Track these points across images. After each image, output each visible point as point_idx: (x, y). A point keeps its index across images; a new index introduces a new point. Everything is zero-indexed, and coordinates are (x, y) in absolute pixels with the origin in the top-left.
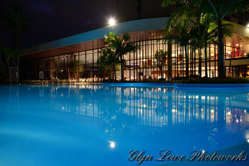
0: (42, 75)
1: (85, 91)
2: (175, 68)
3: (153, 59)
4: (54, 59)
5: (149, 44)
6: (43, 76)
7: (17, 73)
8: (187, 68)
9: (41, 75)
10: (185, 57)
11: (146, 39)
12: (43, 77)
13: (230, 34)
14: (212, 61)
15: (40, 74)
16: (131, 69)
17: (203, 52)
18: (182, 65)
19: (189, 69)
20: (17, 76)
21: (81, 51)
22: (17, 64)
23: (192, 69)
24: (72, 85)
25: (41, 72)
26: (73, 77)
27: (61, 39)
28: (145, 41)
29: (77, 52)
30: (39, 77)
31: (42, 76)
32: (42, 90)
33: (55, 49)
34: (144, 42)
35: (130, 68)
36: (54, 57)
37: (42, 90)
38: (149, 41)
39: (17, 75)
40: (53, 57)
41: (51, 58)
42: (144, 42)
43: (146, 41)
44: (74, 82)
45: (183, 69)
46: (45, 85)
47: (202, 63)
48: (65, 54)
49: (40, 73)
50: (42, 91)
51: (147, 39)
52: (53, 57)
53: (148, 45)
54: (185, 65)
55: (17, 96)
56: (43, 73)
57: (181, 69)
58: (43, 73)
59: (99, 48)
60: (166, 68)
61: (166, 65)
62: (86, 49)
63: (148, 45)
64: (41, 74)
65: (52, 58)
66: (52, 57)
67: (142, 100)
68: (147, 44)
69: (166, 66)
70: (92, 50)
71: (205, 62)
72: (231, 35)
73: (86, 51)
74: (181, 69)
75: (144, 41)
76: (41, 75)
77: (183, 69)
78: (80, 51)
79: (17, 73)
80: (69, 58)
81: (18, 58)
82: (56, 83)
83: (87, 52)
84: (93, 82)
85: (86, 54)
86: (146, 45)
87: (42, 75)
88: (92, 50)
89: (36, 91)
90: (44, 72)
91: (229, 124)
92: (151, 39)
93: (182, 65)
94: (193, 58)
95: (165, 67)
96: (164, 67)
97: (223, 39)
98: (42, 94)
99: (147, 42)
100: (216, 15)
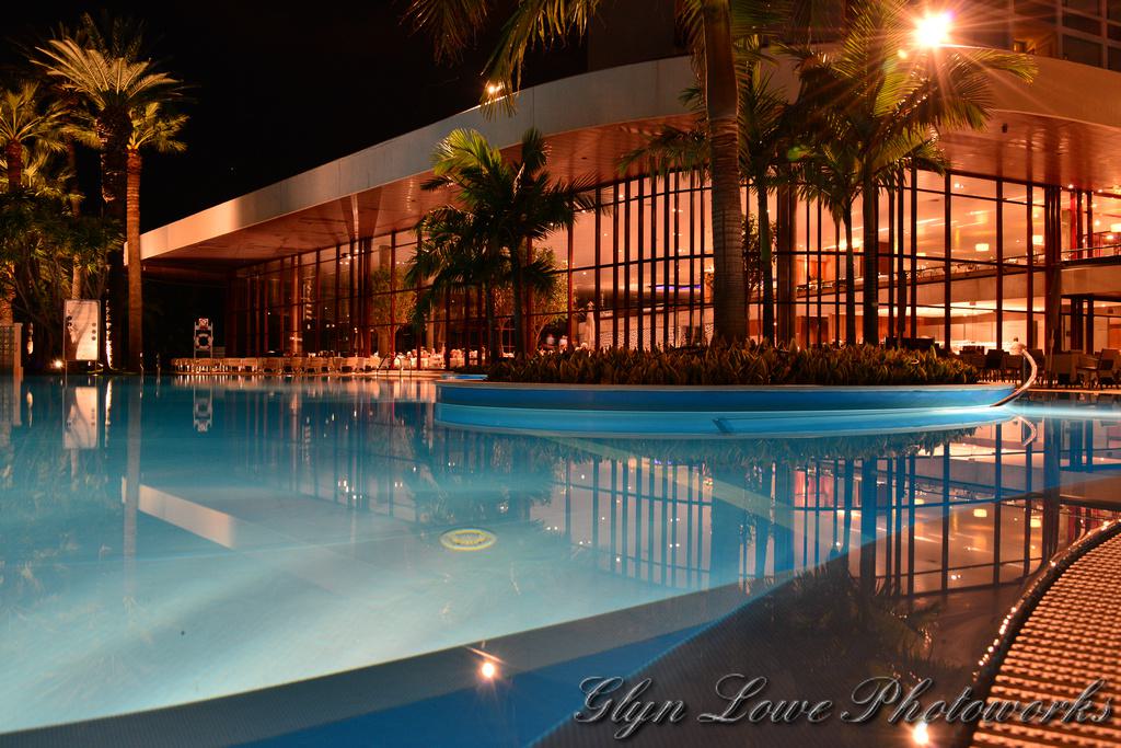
0: (206, 335)
2: (837, 303)
3: (699, 259)
4: (300, 266)
5: (680, 189)
6: (211, 340)
10: (712, 252)
13: (977, 112)
14: (1020, 269)
17: (1038, 219)
19: (1043, 309)
23: (896, 310)
24: (361, 379)
25: (204, 322)
26: (372, 347)
27: (294, 178)
30: (193, 342)
31: (204, 341)
32: (205, 400)
34: (634, 185)
35: (653, 309)
37: (204, 401)
40: (622, 186)
42: (634, 185)
44: (369, 369)
45: (913, 311)
47: (880, 291)
49: (197, 328)
50: (203, 408)
52: (622, 186)
53: (677, 192)
54: (862, 293)
56: (210, 328)
57: (891, 312)
58: (210, 328)
60: (808, 303)
61: (810, 293)
63: (677, 192)
64: (203, 332)
68: (672, 189)
69: (808, 296)
71: (994, 276)
72: (982, 117)
74: (891, 312)
77: (913, 311)
83: (398, 235)
86: (667, 193)
87: (206, 335)
96: (811, 299)
98: (203, 419)
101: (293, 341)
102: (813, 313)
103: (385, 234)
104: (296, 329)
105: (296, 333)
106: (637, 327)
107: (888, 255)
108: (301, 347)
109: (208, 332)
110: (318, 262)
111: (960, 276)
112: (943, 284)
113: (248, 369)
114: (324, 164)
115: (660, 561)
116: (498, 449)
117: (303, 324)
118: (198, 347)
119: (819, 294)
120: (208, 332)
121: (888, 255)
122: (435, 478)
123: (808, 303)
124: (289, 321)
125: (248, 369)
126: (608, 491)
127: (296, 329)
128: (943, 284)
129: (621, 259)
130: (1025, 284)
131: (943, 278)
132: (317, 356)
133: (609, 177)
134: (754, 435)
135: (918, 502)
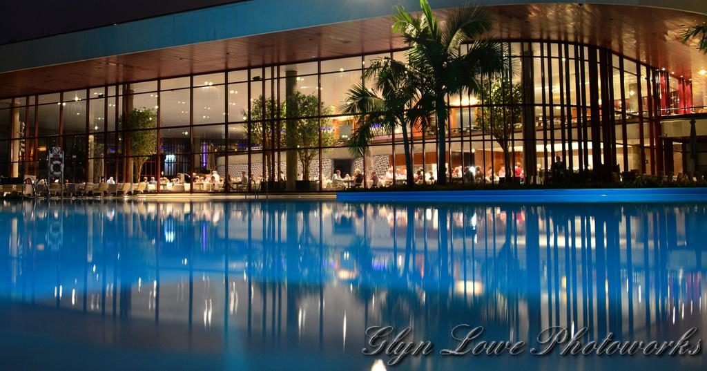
0: (58, 162)
1: (189, 229)
8: (530, 143)
9: (55, 162)
11: (273, 59)
15: (53, 159)
16: (645, 124)
18: (548, 133)
21: (169, 75)
28: (270, 68)
29: (102, 86)
33: (65, 65)
34: (268, 70)
38: (109, 88)
43: (272, 65)
51: (275, 61)
56: (61, 156)
58: (61, 156)
59: (253, 64)
60: (462, 141)
62: (192, 70)
67: (641, 246)
69: (462, 137)
70: (224, 73)
73: (192, 75)
75: (268, 66)
76: (55, 162)
78: (163, 75)
80: (112, 105)
84: (227, 189)
85: (192, 88)
86: (273, 79)
88: (224, 73)
90: (64, 149)
91: (308, 295)
92: (391, 47)
93: (548, 133)
94: (584, 107)
95: (468, 138)
96: (465, 139)
99: (276, 68)
102: (466, 150)
107: (530, 105)
109: (60, 160)
111: (87, 304)
112: (542, 132)
115: (575, 104)
119: (449, 138)
120: (60, 160)
121: (530, 105)
123: (462, 141)
126: (516, 140)
128: (542, 132)
129: (276, 81)
130: (638, 130)
131: (537, 142)
134: (437, 192)
135: (559, 108)
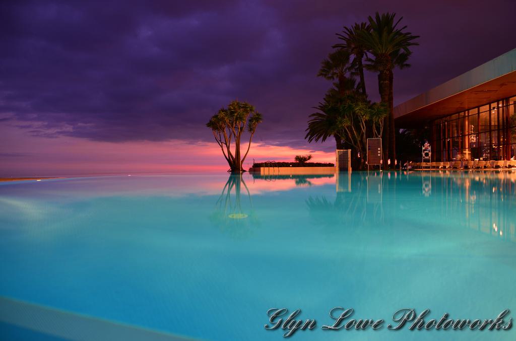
0: (428, 152)
4: (468, 116)
6: (430, 154)
7: (379, 149)
9: (425, 152)
12: (430, 155)
15: (424, 150)
20: (379, 155)
22: (379, 134)
30: (422, 155)
31: (427, 155)
36: (468, 110)
37: (427, 183)
39: (380, 153)
40: (467, 112)
41: (462, 114)
46: (445, 172)
48: (481, 106)
49: (423, 148)
52: (467, 112)
55: (379, 192)
58: (430, 148)
64: (426, 150)
65: (465, 113)
66: (464, 111)
76: (425, 152)
79: (379, 149)
81: (364, 128)
82: (466, 167)
89: (417, 184)
97: (451, 194)
100: (351, 143)
101: (465, 153)
103: (474, 108)
104: (467, 147)
105: (467, 150)
106: (276, 168)
108: (470, 156)
110: (479, 113)
113: (444, 167)
114: (478, 65)
116: (293, 161)
117: (470, 144)
118: (424, 157)
122: (352, 174)
124: (463, 143)
125: (444, 167)
127: (467, 147)
132: (479, 160)
133: (467, 108)
